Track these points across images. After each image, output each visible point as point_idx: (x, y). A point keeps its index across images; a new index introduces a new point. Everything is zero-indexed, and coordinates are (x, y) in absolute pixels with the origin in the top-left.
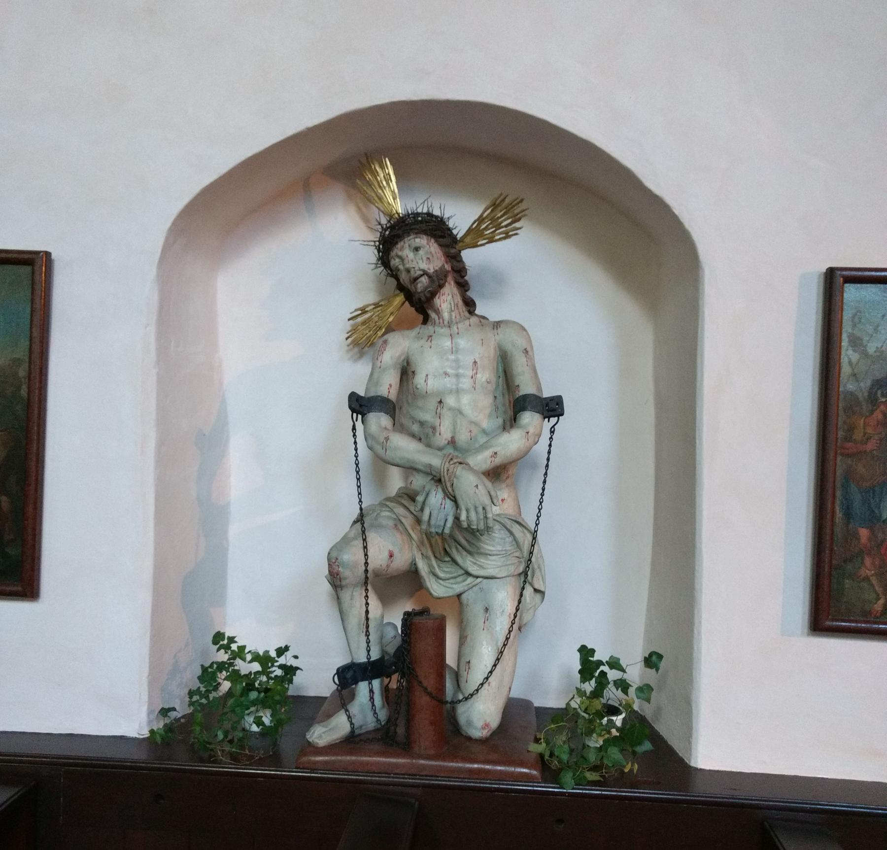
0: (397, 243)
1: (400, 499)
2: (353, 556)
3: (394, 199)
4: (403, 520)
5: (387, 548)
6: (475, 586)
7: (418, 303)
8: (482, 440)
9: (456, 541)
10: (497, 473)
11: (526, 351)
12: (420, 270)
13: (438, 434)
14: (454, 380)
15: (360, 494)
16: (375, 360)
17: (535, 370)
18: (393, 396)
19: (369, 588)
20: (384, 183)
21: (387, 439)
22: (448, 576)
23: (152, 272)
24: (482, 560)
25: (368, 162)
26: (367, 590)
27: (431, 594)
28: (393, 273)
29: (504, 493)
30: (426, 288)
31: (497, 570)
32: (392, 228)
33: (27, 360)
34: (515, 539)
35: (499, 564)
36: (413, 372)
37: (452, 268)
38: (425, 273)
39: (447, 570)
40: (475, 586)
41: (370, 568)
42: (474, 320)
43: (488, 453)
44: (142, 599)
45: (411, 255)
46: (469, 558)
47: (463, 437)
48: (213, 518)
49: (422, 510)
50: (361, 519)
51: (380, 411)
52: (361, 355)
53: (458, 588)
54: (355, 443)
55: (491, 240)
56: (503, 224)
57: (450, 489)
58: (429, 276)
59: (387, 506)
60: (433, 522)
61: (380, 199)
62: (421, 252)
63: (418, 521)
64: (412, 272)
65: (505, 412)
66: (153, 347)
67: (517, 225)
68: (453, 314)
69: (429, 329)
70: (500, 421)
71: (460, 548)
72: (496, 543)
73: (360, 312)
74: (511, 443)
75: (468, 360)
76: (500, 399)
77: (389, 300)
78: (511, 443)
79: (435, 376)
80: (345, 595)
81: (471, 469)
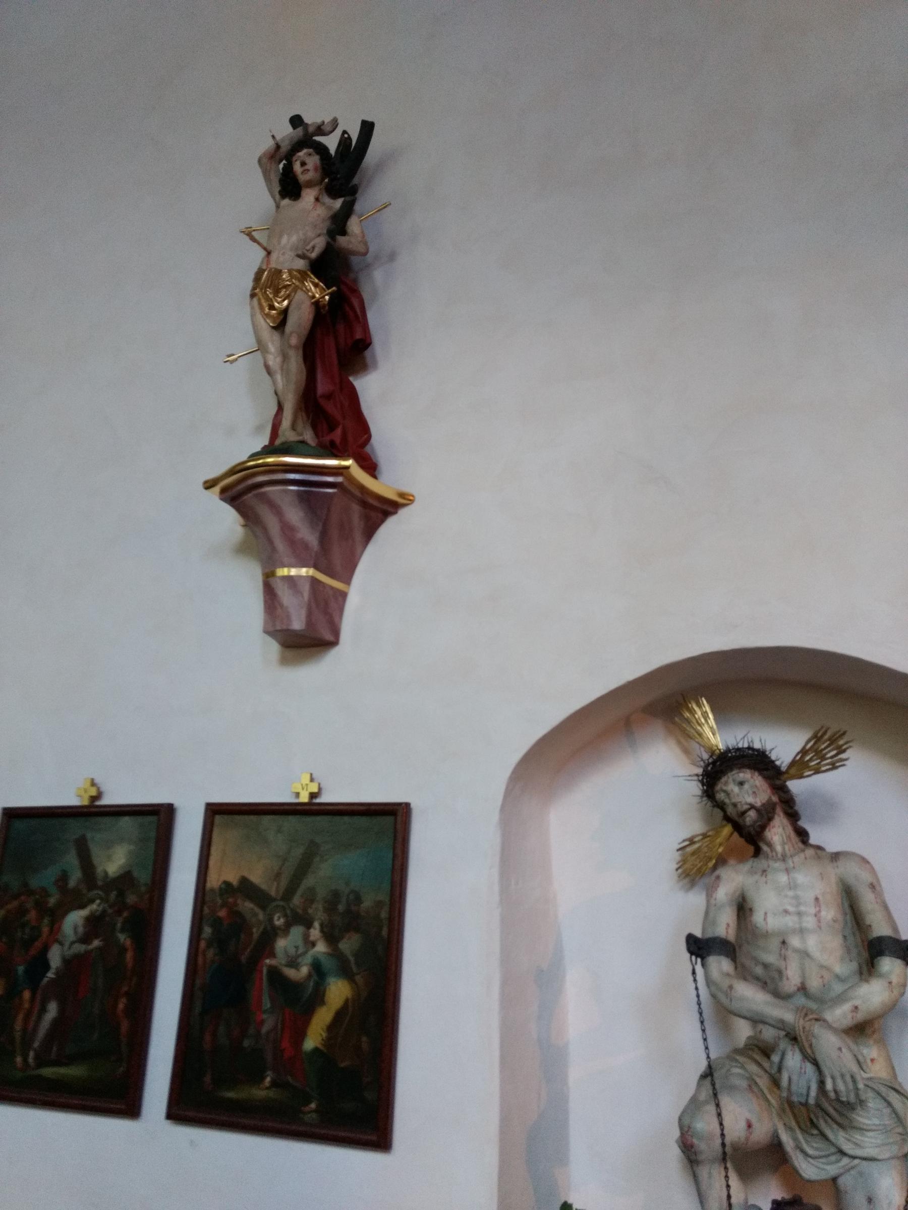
0: (720, 778)
1: (750, 1053)
2: (705, 1124)
3: (714, 734)
4: (758, 1080)
5: (743, 1116)
6: (853, 1168)
7: (749, 837)
8: (838, 988)
9: (823, 1110)
10: (861, 1029)
11: (872, 886)
12: (747, 804)
13: (785, 978)
14: (796, 918)
15: (707, 1048)
16: (710, 891)
17: (886, 908)
18: (731, 937)
19: (729, 1165)
20: (703, 720)
21: (731, 987)
22: (816, 1153)
23: (495, 817)
24: (858, 1137)
25: (685, 701)
26: (726, 1168)
27: (800, 1176)
28: (721, 806)
29: (870, 1051)
30: (755, 822)
31: (877, 1150)
32: (714, 763)
33: (388, 903)
34: (894, 1111)
35: (879, 1141)
36: (751, 910)
37: (780, 799)
38: (752, 807)
39: (815, 1145)
40: (853, 1168)
41: (728, 1140)
42: (810, 852)
43: (847, 1007)
44: (489, 1158)
45: (736, 789)
46: (841, 1133)
47: (814, 984)
48: (553, 1062)
49: (780, 1070)
50: (708, 1074)
51: (720, 954)
52: (692, 884)
53: (832, 1170)
54: (697, 989)
55: (817, 771)
56: (829, 755)
57: (809, 1051)
58: (758, 810)
59: (737, 1061)
60: (794, 1088)
61: (700, 735)
62: (746, 786)
63: (775, 1082)
64: (739, 806)
65: (859, 954)
66: (496, 888)
67: (843, 756)
68: (787, 847)
69: (761, 863)
70: (854, 966)
71: (829, 1120)
72: (872, 1116)
73: (687, 843)
74: (873, 995)
75: (808, 896)
76: (851, 939)
77: (717, 831)
78: (873, 995)
79: (775, 915)
80: (702, 1172)
81: (829, 1027)
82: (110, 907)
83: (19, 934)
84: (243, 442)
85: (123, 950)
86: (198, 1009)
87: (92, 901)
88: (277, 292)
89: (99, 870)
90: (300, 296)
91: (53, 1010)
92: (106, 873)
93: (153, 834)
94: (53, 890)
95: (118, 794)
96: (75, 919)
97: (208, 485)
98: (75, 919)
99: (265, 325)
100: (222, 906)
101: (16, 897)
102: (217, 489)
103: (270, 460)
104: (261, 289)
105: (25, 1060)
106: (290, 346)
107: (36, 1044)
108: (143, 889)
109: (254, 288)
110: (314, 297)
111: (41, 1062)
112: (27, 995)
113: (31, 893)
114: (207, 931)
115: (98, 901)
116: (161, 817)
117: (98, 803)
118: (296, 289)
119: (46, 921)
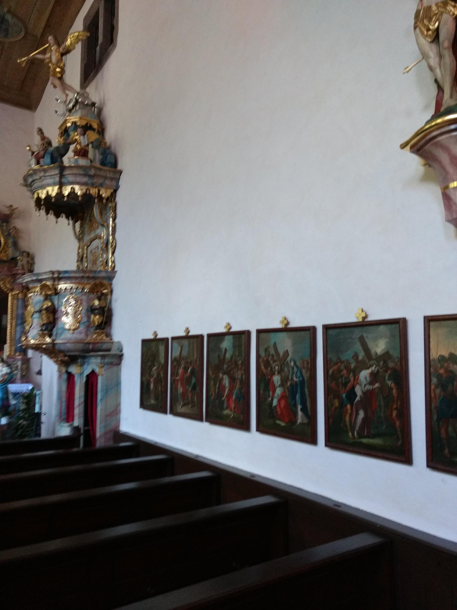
82: (381, 368)
83: (340, 380)
84: (418, 116)
85: (391, 389)
86: (435, 417)
87: (371, 366)
88: (430, 20)
89: (373, 352)
90: (445, 16)
91: (361, 414)
92: (376, 353)
93: (398, 333)
94: (352, 361)
95: (375, 315)
96: (364, 375)
97: (402, 146)
98: (364, 375)
99: (425, 43)
100: (441, 368)
101: (336, 364)
102: (408, 147)
103: (439, 121)
104: (420, 22)
105: (353, 434)
106: (444, 49)
107: (357, 428)
108: (396, 360)
109: (415, 23)
110: (454, 14)
111: (361, 436)
112: (349, 406)
113: (342, 362)
114: (434, 380)
115: (374, 366)
116: (399, 326)
117: (366, 320)
118: (442, 14)
119: (351, 374)
